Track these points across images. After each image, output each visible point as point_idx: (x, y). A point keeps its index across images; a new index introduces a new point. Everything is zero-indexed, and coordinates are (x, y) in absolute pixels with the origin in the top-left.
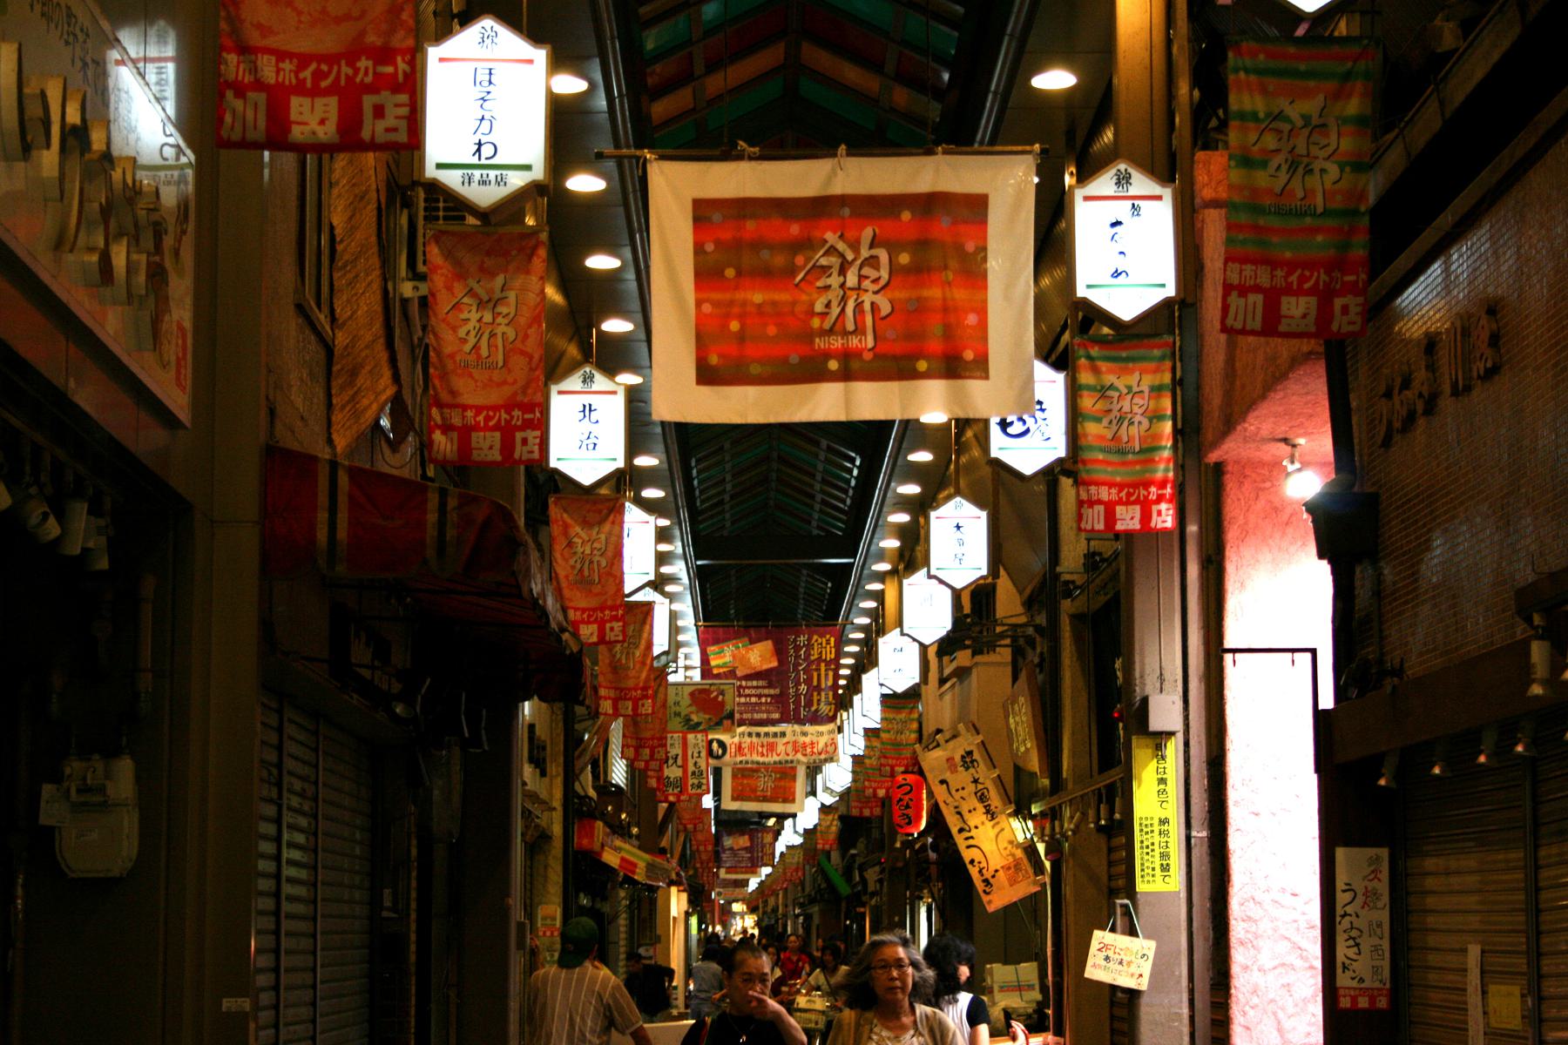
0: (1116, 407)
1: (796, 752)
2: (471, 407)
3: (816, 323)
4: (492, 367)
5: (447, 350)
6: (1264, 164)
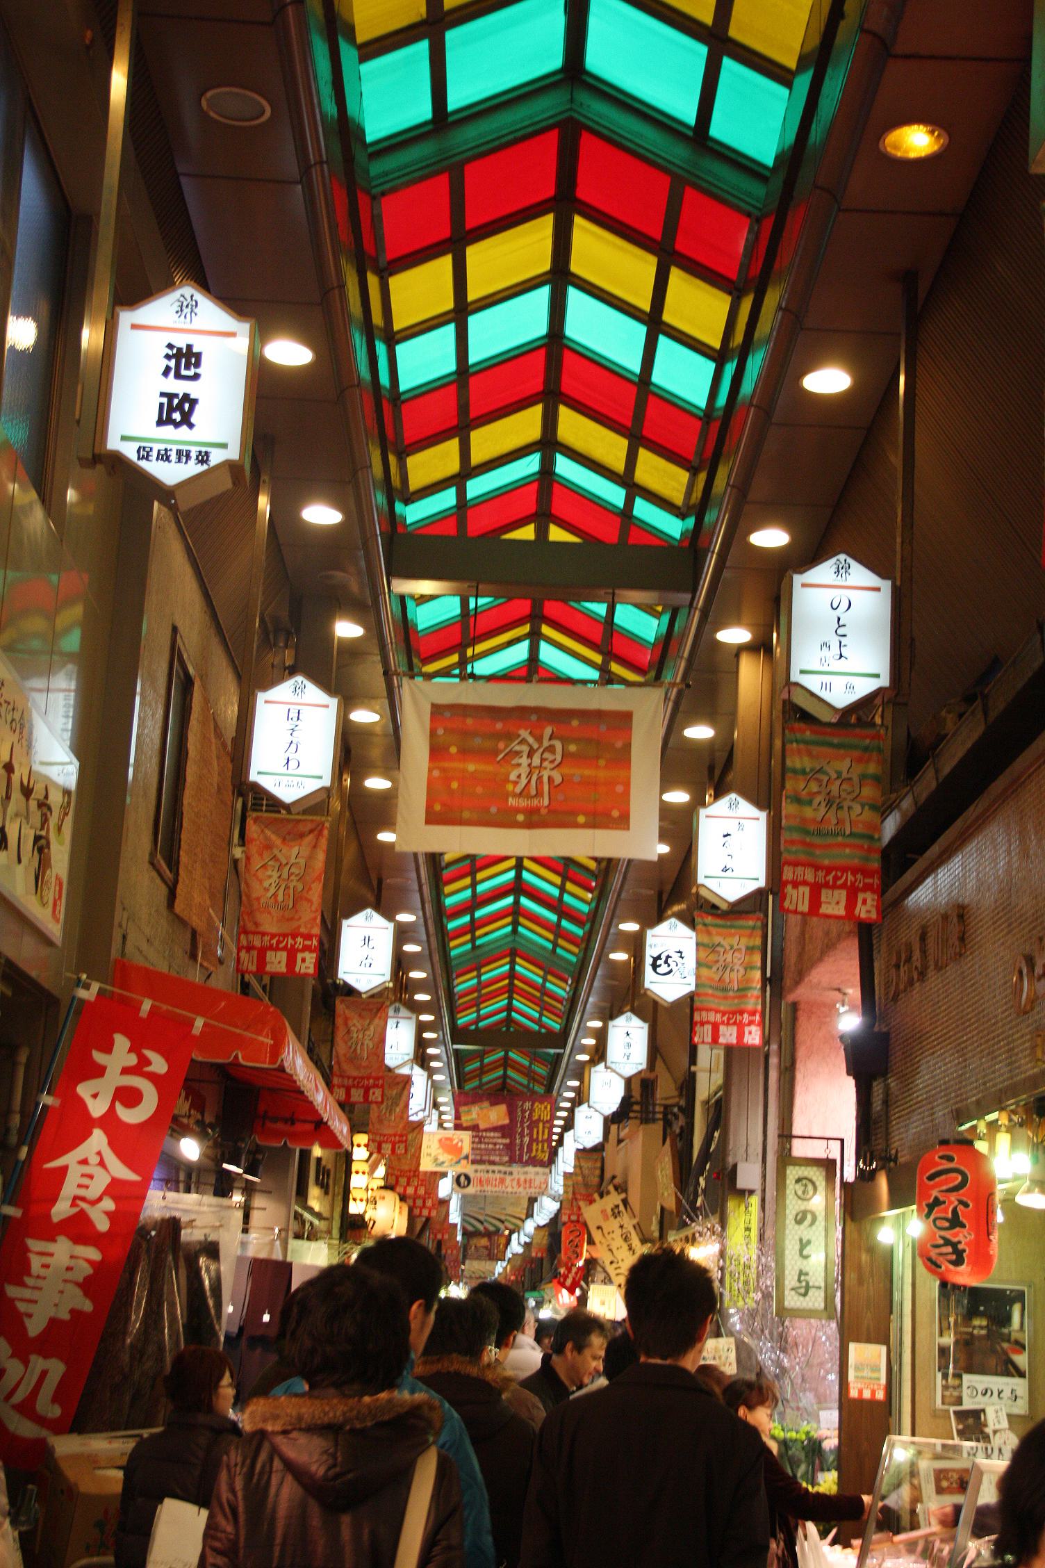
0: (722, 959)
1: (519, 1186)
2: (268, 934)
3: (510, 787)
4: (285, 908)
5: (255, 895)
6: (810, 803)
